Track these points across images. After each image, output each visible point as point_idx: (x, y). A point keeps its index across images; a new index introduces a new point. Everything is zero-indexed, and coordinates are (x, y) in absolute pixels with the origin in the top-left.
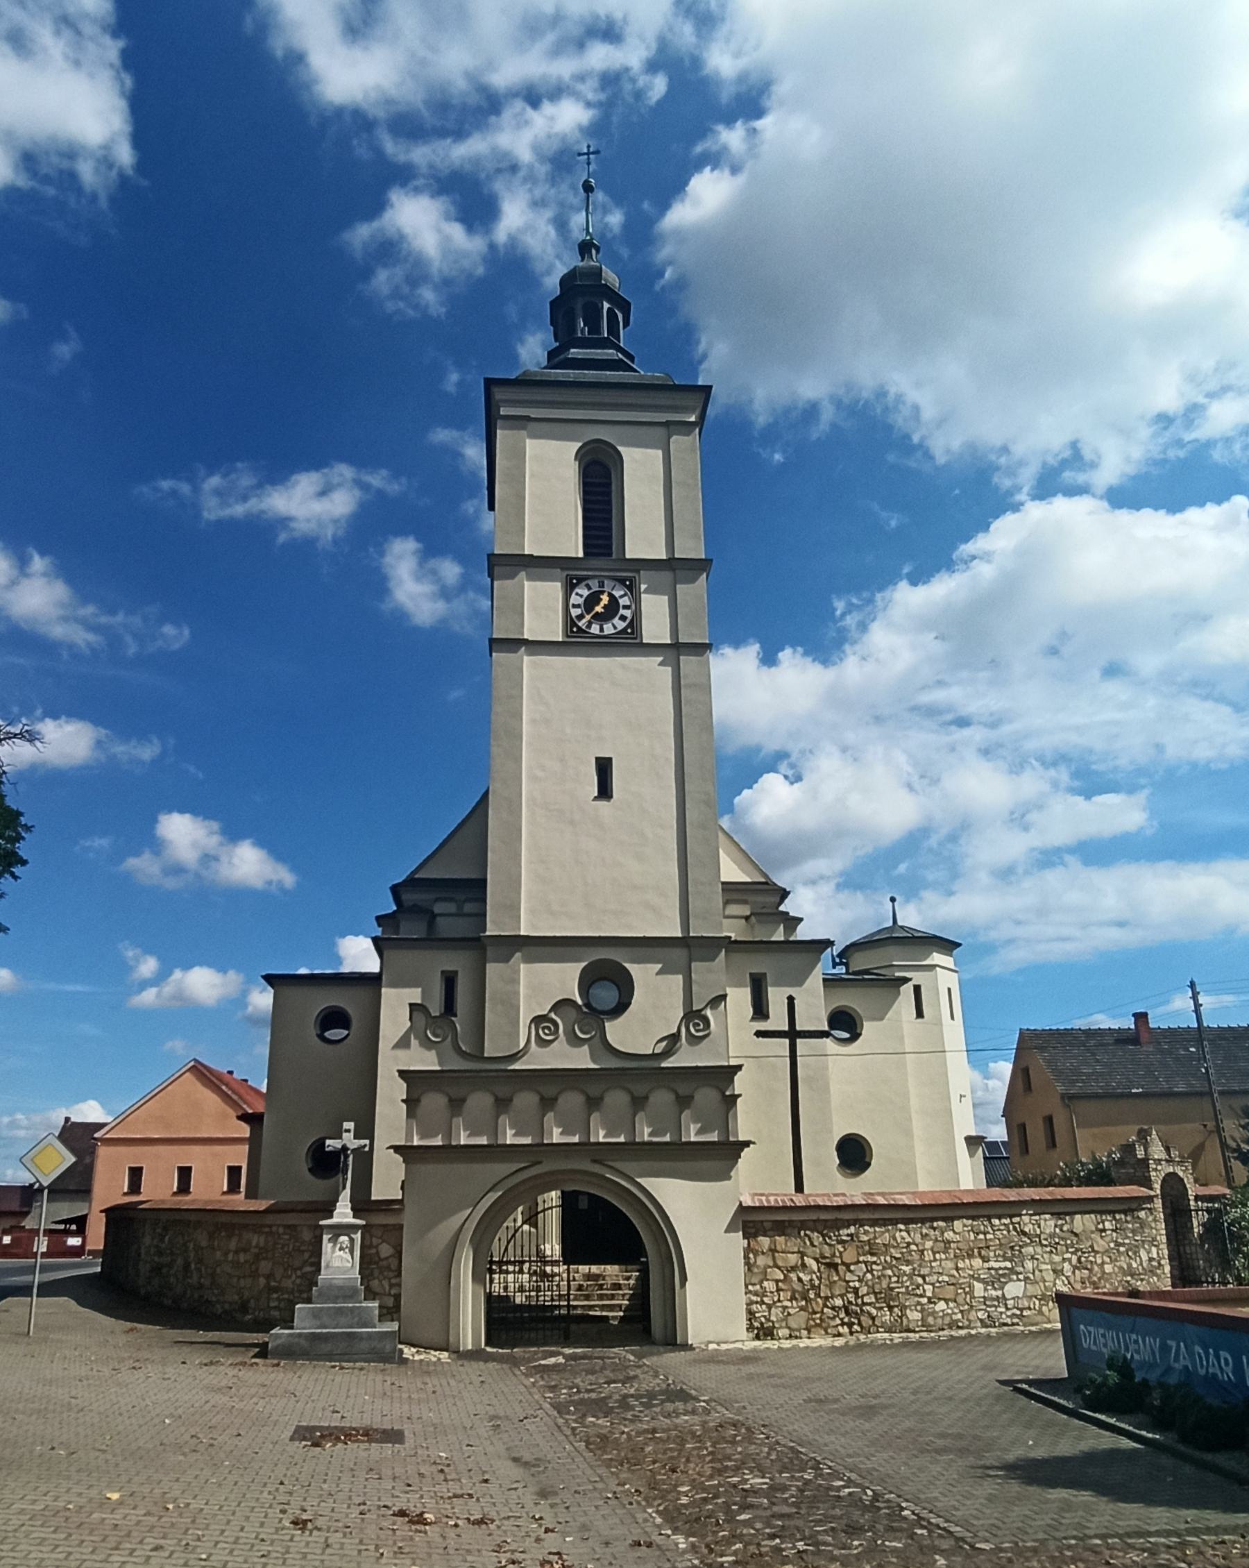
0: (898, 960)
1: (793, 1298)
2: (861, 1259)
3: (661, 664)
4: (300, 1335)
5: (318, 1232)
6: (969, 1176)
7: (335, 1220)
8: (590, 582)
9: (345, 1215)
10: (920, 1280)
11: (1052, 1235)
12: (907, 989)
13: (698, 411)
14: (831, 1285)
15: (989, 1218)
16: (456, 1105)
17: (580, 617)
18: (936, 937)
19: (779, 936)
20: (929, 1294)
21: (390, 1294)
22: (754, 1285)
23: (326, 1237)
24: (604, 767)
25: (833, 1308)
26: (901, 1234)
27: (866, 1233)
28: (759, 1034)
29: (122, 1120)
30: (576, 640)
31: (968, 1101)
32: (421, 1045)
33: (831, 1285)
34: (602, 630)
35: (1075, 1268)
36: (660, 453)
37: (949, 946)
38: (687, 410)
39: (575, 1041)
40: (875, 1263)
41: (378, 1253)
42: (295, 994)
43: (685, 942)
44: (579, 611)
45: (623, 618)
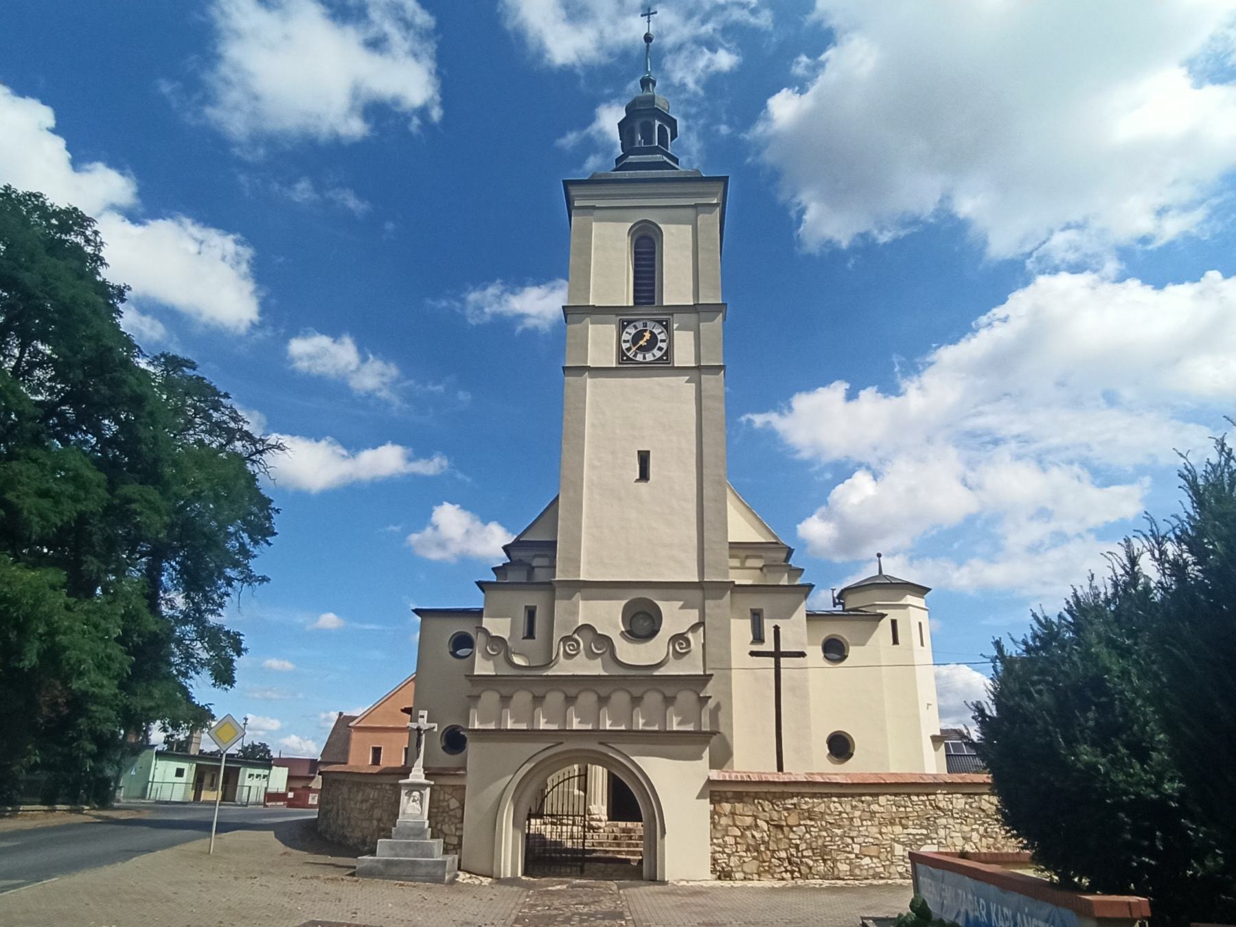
0: (876, 599)
1: (747, 850)
3: (687, 382)
4: (378, 861)
5: (397, 789)
6: (933, 764)
7: (411, 780)
8: (636, 324)
9: (418, 777)
10: (850, 841)
11: (963, 811)
12: (886, 624)
13: (720, 195)
14: (778, 841)
15: (909, 795)
16: (506, 700)
17: (629, 349)
18: (908, 583)
19: (784, 581)
20: (857, 851)
23: (403, 792)
24: (644, 458)
25: (779, 859)
26: (835, 805)
27: (806, 803)
28: (753, 654)
29: (367, 715)
30: (626, 365)
31: (934, 710)
32: (483, 657)
33: (778, 841)
35: (982, 836)
36: (690, 228)
37: (921, 591)
38: (713, 195)
39: (591, 655)
42: (435, 623)
43: (700, 585)
44: (628, 345)
45: (660, 349)
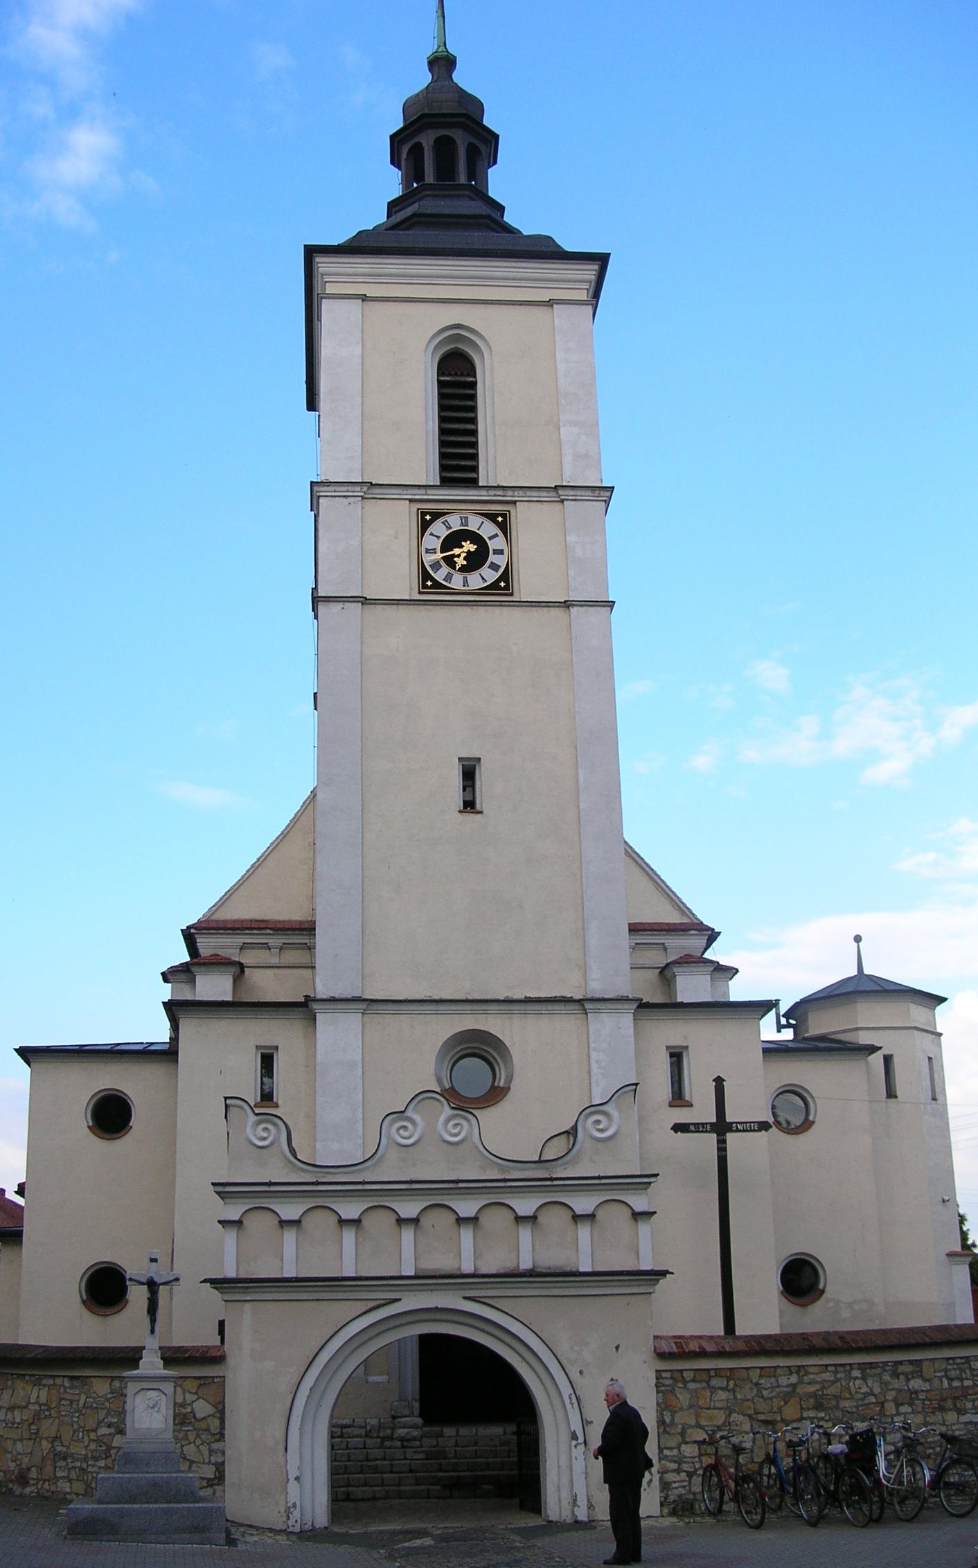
2: (805, 1415)
8: (450, 518)
21: (209, 1463)
22: (671, 1449)
28: (679, 1128)
34: (466, 583)
40: (823, 1419)
41: (193, 1412)
45: (494, 567)
